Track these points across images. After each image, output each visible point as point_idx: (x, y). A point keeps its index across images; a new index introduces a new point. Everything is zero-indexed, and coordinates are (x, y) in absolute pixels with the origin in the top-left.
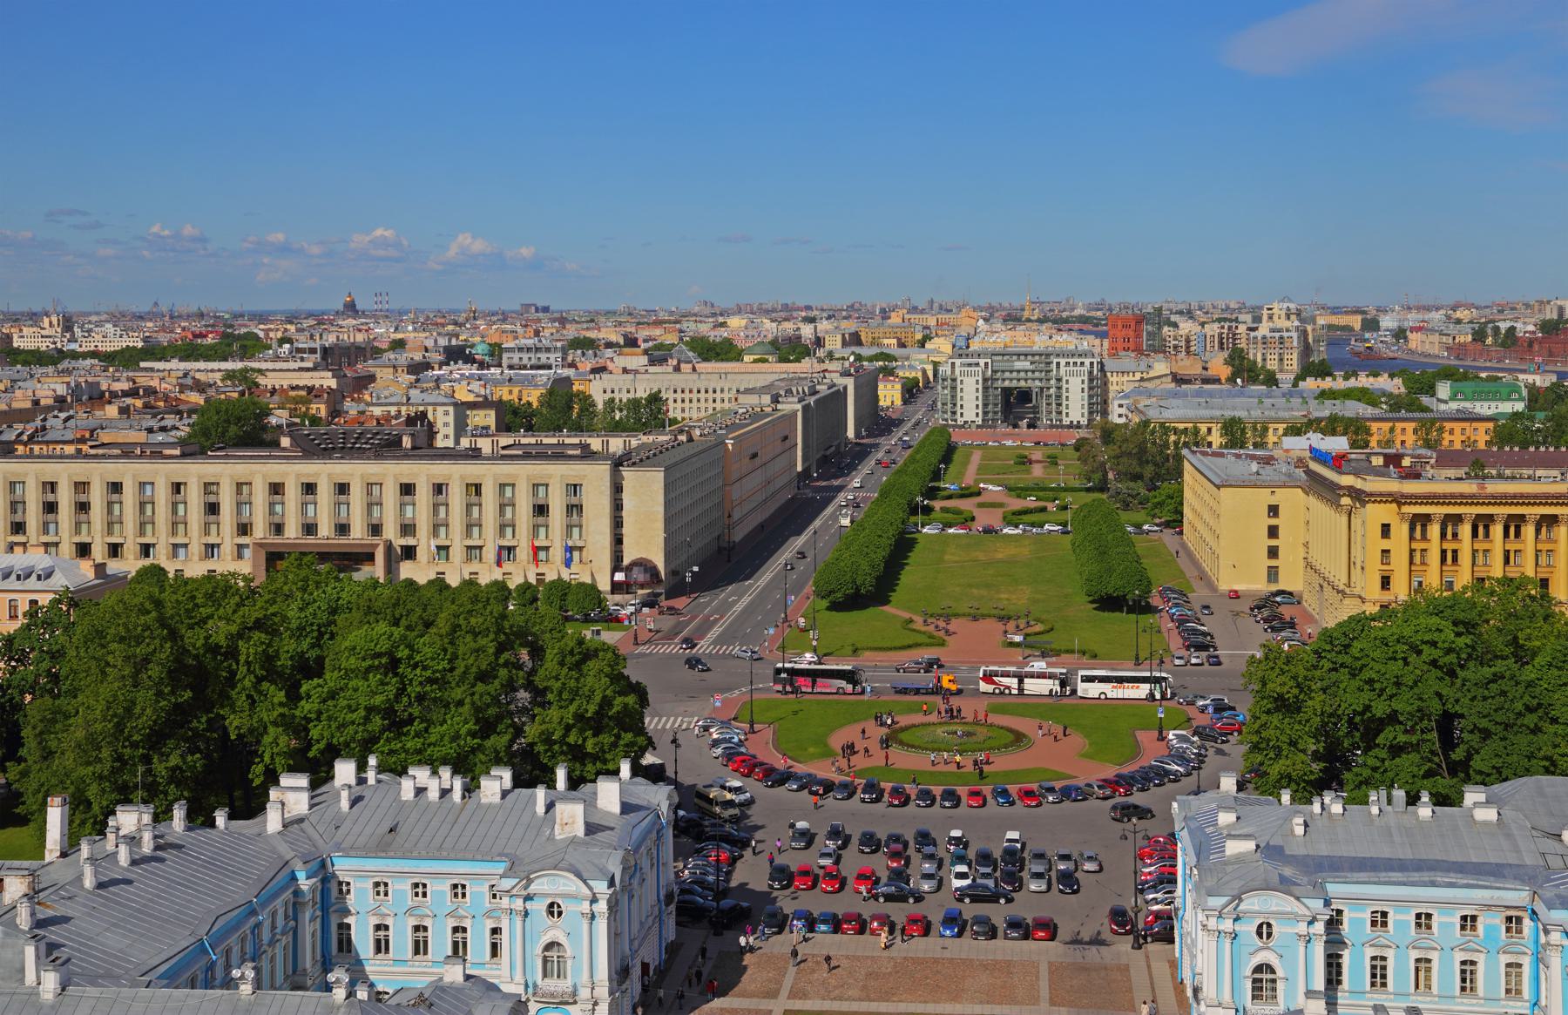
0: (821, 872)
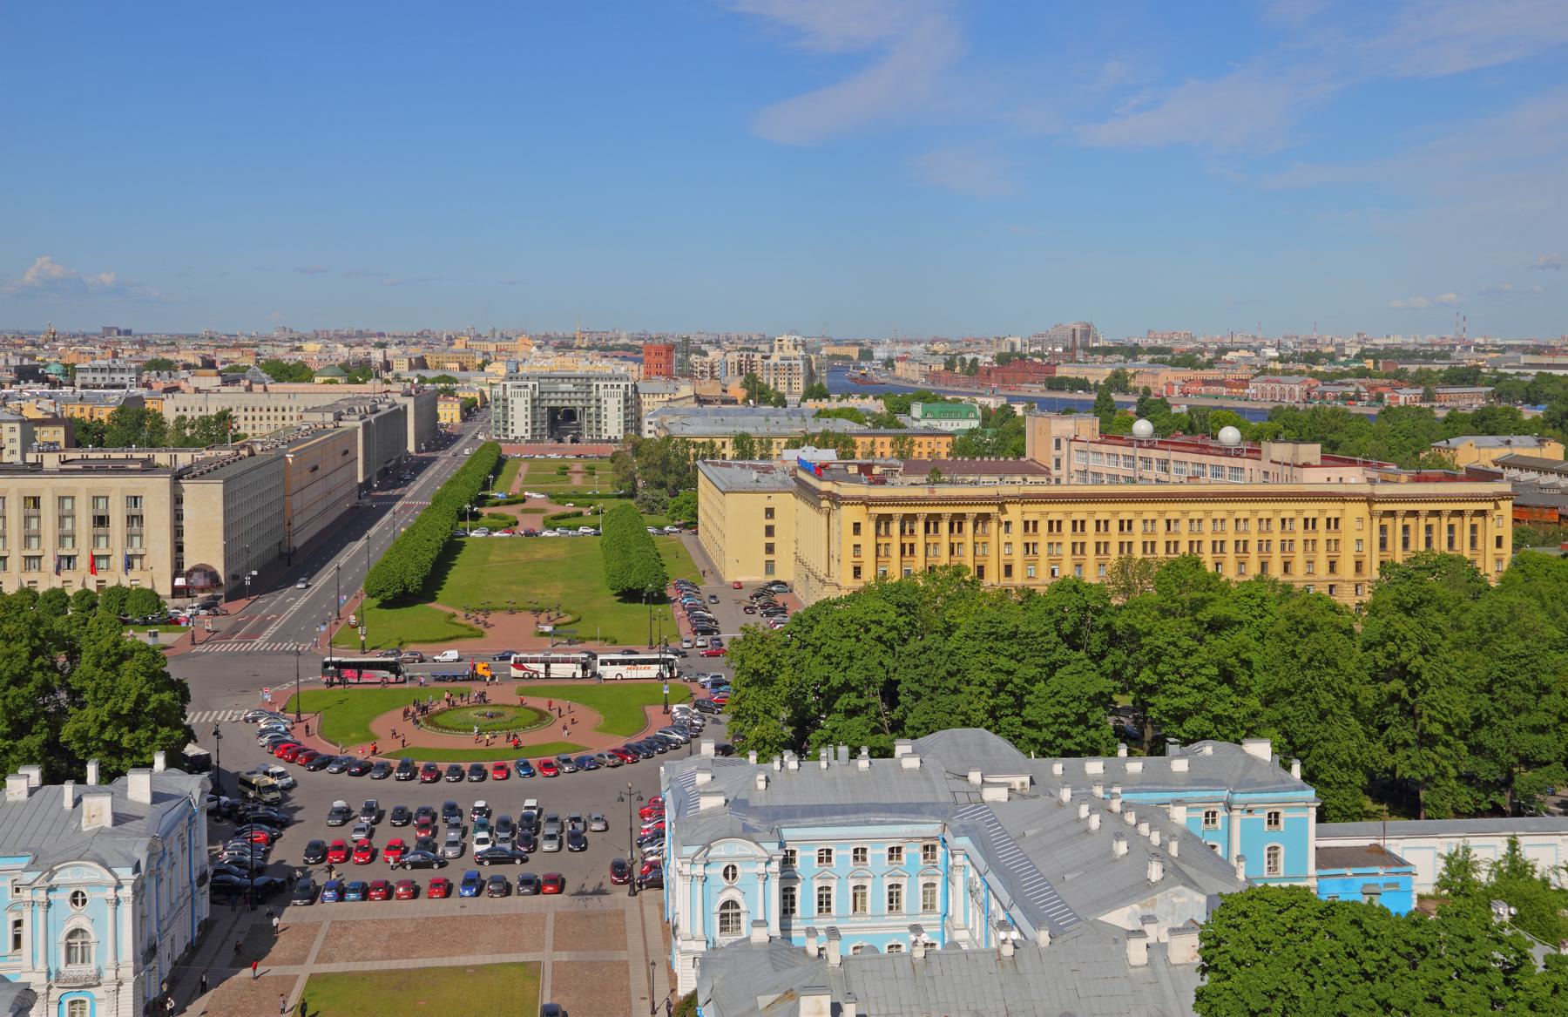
0: (354, 846)
